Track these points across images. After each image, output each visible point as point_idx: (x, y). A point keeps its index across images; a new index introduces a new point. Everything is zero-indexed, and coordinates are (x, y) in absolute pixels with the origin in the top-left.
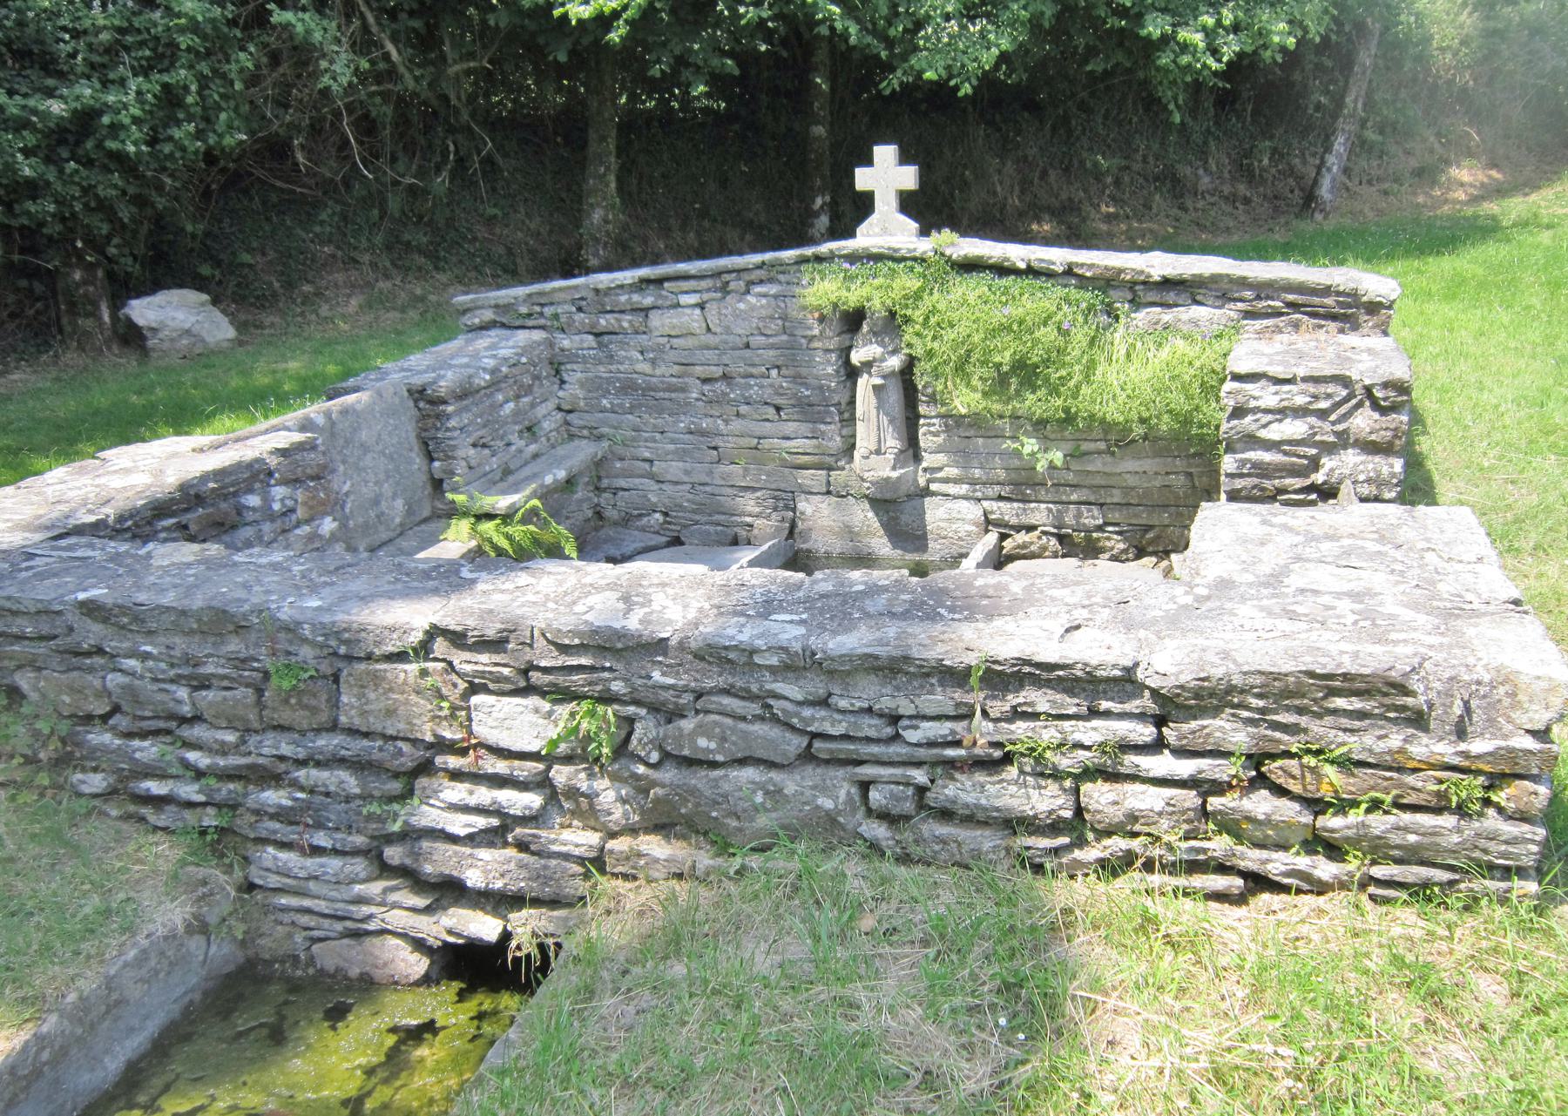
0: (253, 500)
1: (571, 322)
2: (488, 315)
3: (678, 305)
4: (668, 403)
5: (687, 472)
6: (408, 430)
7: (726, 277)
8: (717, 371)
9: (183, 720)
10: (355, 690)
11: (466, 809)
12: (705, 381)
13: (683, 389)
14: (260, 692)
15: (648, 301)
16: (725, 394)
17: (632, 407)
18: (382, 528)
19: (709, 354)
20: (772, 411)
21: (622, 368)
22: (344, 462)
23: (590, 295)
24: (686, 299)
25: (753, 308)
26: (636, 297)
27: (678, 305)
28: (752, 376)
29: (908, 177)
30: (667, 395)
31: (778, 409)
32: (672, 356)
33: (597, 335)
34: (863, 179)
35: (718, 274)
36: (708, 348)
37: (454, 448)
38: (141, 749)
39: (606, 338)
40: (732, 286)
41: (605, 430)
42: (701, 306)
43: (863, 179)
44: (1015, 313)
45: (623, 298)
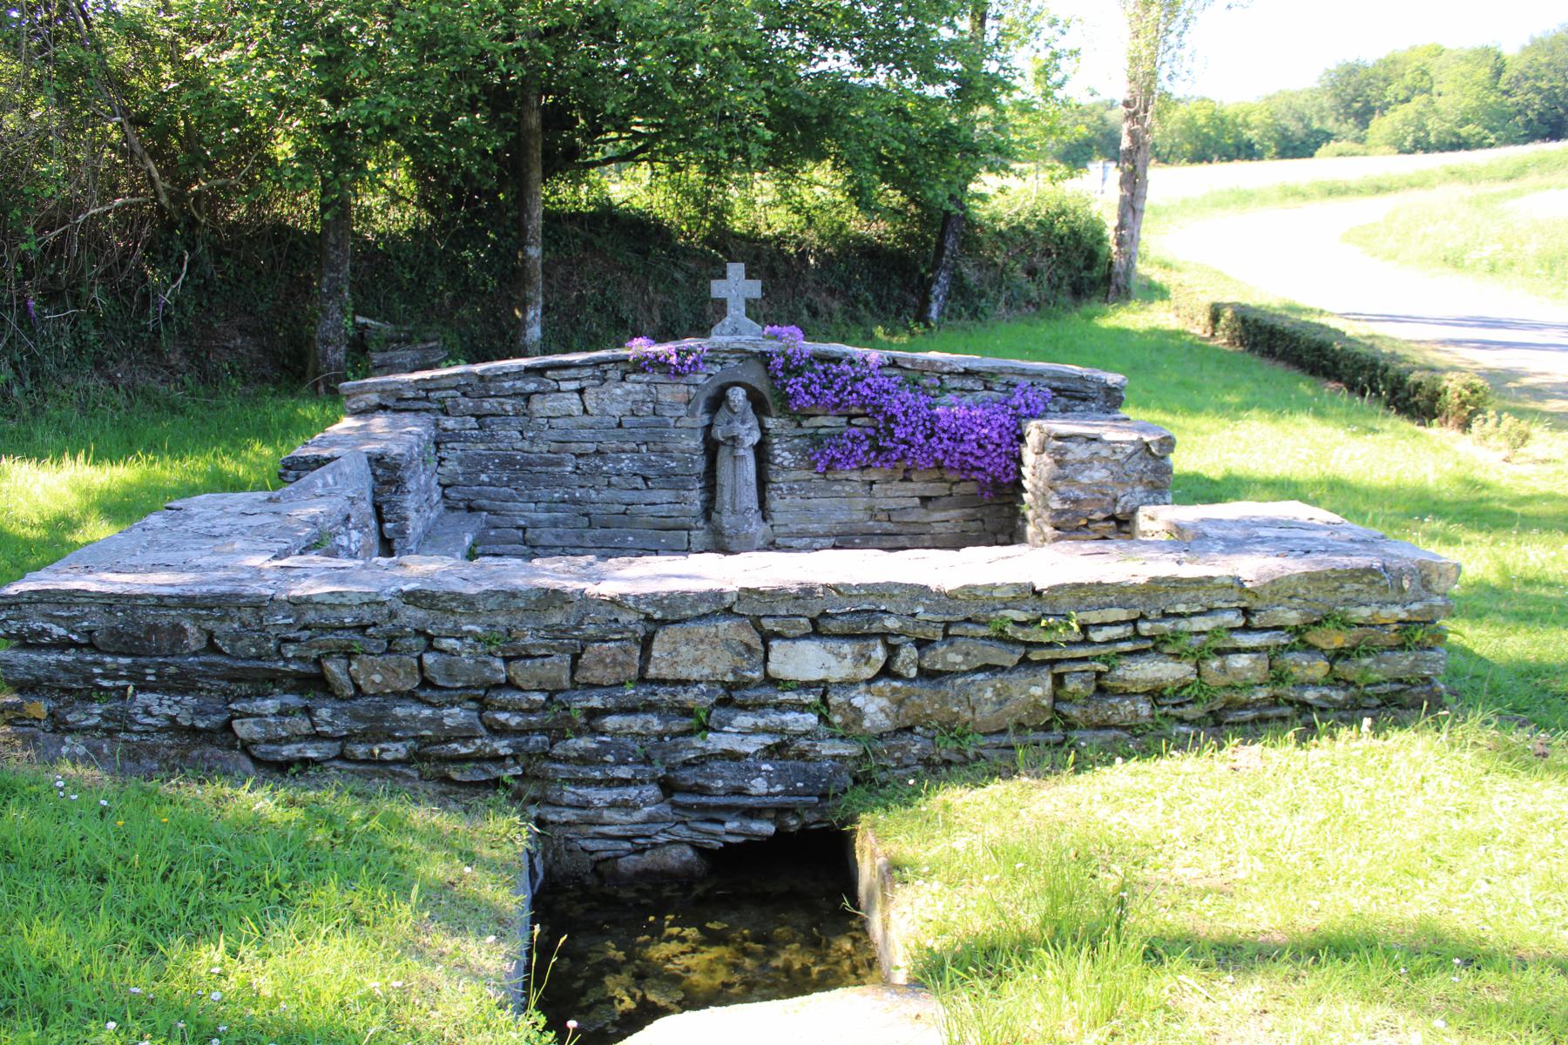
2: (374, 398)
3: (559, 391)
4: (544, 476)
5: (557, 536)
7: (606, 367)
8: (591, 448)
9: (498, 686)
10: (667, 646)
11: (755, 731)
12: (579, 456)
14: (576, 658)
15: (532, 387)
16: (597, 467)
17: (510, 480)
19: (585, 433)
20: (640, 480)
21: (501, 446)
23: (475, 381)
24: (564, 386)
25: (629, 393)
26: (519, 384)
27: (559, 391)
28: (624, 451)
29: (755, 289)
30: (544, 469)
31: (646, 479)
32: (554, 435)
33: (478, 417)
34: (718, 288)
35: (597, 364)
36: (583, 427)
38: (449, 716)
39: (488, 420)
40: (610, 374)
43: (718, 288)
45: (507, 385)
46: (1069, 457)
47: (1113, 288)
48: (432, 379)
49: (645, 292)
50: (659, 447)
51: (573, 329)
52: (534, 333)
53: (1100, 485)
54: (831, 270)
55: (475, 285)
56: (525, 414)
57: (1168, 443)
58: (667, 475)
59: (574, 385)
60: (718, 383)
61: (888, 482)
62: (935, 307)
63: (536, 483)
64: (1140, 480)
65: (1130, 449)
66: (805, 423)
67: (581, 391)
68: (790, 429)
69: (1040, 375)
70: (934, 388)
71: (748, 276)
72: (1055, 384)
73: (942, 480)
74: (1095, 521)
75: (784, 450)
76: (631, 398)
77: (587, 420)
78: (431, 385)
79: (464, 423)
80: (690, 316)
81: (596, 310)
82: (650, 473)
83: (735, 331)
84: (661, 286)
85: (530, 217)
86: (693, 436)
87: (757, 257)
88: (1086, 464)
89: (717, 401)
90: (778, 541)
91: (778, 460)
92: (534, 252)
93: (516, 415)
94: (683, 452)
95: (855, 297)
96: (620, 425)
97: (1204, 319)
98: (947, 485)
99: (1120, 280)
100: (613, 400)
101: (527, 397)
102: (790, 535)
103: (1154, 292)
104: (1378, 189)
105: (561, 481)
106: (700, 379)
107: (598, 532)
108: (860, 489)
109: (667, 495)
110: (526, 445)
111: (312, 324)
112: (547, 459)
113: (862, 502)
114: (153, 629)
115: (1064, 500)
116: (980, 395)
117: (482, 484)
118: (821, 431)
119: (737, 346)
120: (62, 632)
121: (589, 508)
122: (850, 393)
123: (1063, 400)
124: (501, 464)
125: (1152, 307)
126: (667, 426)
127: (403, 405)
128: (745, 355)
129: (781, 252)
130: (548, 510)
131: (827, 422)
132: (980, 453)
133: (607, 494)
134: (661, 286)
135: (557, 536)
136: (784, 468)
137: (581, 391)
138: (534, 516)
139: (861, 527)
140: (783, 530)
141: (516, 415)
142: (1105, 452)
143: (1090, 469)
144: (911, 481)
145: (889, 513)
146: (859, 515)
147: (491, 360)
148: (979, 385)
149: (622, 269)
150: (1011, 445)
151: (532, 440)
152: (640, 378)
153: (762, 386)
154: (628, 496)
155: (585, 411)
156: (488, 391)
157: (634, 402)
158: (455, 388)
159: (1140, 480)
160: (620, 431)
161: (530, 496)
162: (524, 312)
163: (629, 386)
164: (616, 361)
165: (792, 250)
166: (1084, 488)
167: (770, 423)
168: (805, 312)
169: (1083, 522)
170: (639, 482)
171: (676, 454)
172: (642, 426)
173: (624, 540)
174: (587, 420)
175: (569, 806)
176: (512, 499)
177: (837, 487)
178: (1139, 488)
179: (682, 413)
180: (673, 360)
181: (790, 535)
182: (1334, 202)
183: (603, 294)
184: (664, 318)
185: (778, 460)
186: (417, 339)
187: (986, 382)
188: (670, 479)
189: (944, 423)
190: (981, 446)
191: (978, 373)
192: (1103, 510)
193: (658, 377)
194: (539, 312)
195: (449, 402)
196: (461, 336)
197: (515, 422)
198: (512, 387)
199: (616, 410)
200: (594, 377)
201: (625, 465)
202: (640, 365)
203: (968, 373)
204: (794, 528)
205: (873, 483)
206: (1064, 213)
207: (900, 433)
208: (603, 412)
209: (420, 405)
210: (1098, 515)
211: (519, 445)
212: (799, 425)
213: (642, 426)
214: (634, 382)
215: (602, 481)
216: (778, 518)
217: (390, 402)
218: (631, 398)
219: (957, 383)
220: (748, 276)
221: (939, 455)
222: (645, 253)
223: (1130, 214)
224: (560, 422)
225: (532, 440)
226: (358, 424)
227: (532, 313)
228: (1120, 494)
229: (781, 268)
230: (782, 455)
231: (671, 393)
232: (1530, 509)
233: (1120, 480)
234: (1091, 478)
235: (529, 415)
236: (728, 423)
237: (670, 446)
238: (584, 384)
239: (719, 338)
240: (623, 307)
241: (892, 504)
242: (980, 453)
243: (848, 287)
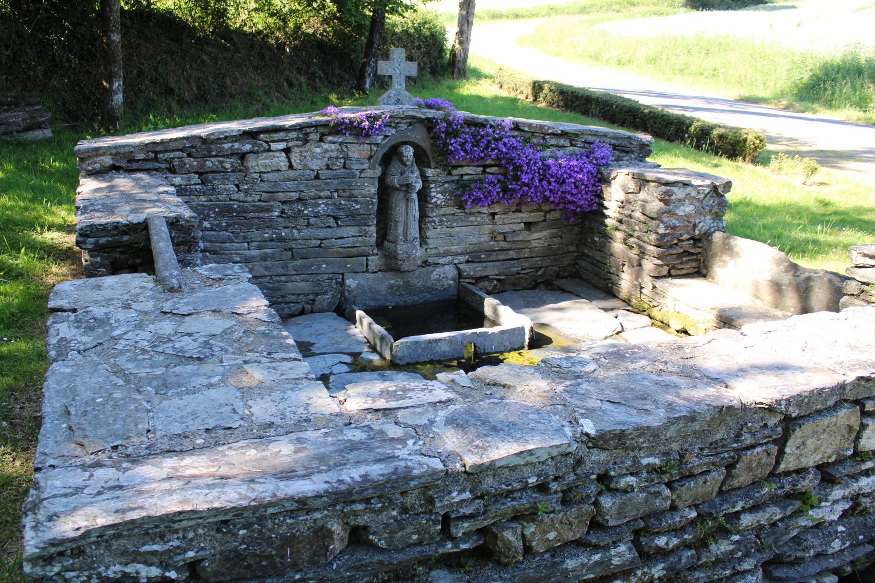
2: (108, 161)
3: (269, 150)
4: (256, 221)
5: (267, 268)
7: (308, 130)
8: (295, 196)
15: (248, 147)
16: (300, 211)
17: (228, 225)
19: (290, 184)
20: (332, 220)
21: (221, 197)
23: (198, 144)
24: (274, 146)
25: (326, 151)
26: (236, 145)
28: (320, 198)
31: (336, 219)
32: (265, 187)
33: (200, 174)
34: (384, 68)
36: (288, 180)
39: (210, 176)
43: (384, 68)
45: (226, 146)
46: (673, 197)
47: (456, 70)
48: (163, 142)
49: (184, 69)
50: (347, 194)
51: (137, 96)
53: (688, 216)
54: (297, 56)
55: (61, 61)
56: (241, 169)
57: (728, 185)
59: (282, 145)
60: (393, 143)
61: (506, 213)
62: (368, 81)
63: (249, 227)
64: (710, 211)
65: (707, 190)
66: (454, 172)
67: (287, 151)
68: (443, 177)
69: (605, 135)
72: (613, 142)
73: (539, 210)
74: (683, 241)
75: (438, 192)
76: (327, 155)
79: (189, 179)
80: (216, 86)
81: (151, 81)
82: (341, 214)
83: (398, 101)
84: (194, 65)
85: (111, 11)
86: (373, 184)
87: (252, 46)
89: (391, 156)
91: (434, 200)
92: (116, 37)
93: (233, 171)
94: (365, 197)
95: (313, 74)
96: (317, 177)
97: (529, 91)
98: (542, 214)
99: (460, 65)
100: (313, 157)
101: (243, 156)
102: (438, 255)
103: (479, 75)
104: (517, 16)
105: (270, 224)
106: (379, 139)
107: (299, 262)
108: (487, 219)
109: (352, 231)
110: (241, 196)
112: (259, 206)
113: (487, 228)
114: (290, 540)
115: (667, 228)
117: (206, 229)
118: (465, 178)
120: (155, 572)
121: (292, 244)
122: (493, 150)
123: (617, 153)
124: (220, 212)
125: (480, 82)
126: (354, 177)
127: (135, 166)
128: (414, 121)
129: (266, 43)
130: (259, 248)
131: (470, 171)
132: (575, 191)
133: (306, 232)
134: (194, 65)
135: (267, 268)
136: (437, 206)
137: (287, 151)
138: (247, 253)
139: (486, 246)
140: (433, 251)
141: (233, 171)
142: (694, 194)
143: (683, 205)
144: (520, 211)
145: (505, 236)
146: (485, 238)
148: (567, 143)
149: (166, 53)
150: (594, 185)
151: (246, 192)
152: (335, 139)
153: (425, 144)
154: (322, 233)
155: (291, 167)
156: (210, 151)
158: (182, 150)
159: (710, 211)
160: (318, 182)
161: (245, 238)
162: (111, 83)
163: (326, 146)
164: (317, 126)
165: (273, 42)
166: (679, 218)
167: (430, 172)
168: (285, 84)
169: (675, 242)
171: (360, 199)
172: (335, 177)
173: (319, 267)
174: (292, 174)
177: (472, 219)
179: (366, 166)
180: (366, 124)
181: (438, 255)
182: (495, 22)
183: (156, 70)
184: (199, 88)
185: (434, 200)
186: (23, 104)
187: (571, 140)
188: (355, 218)
189: (554, 170)
190: (576, 187)
192: (688, 233)
193: (349, 138)
194: (121, 83)
195: (176, 162)
196: (55, 101)
197: (233, 177)
198: (230, 148)
199: (316, 164)
200: (298, 139)
201: (322, 209)
202: (338, 128)
203: (564, 134)
204: (441, 250)
205: (496, 214)
206: (425, 23)
207: (525, 179)
208: (306, 167)
209: (150, 165)
210: (686, 236)
211: (236, 196)
212: (450, 173)
213: (335, 177)
215: (302, 222)
216: (432, 243)
217: (123, 164)
218: (327, 155)
219: (554, 141)
221: (547, 193)
222: (179, 41)
223: (466, 25)
224: (270, 176)
225: (246, 192)
226: (104, 185)
227: (117, 84)
228: (697, 221)
229: (267, 54)
230: (437, 197)
231: (358, 151)
232: (866, 217)
233: (699, 212)
234: (684, 211)
235: (245, 171)
236: (402, 174)
237: (356, 192)
238: (290, 144)
240: (171, 80)
241: (507, 228)
242: (575, 191)
243: (309, 67)
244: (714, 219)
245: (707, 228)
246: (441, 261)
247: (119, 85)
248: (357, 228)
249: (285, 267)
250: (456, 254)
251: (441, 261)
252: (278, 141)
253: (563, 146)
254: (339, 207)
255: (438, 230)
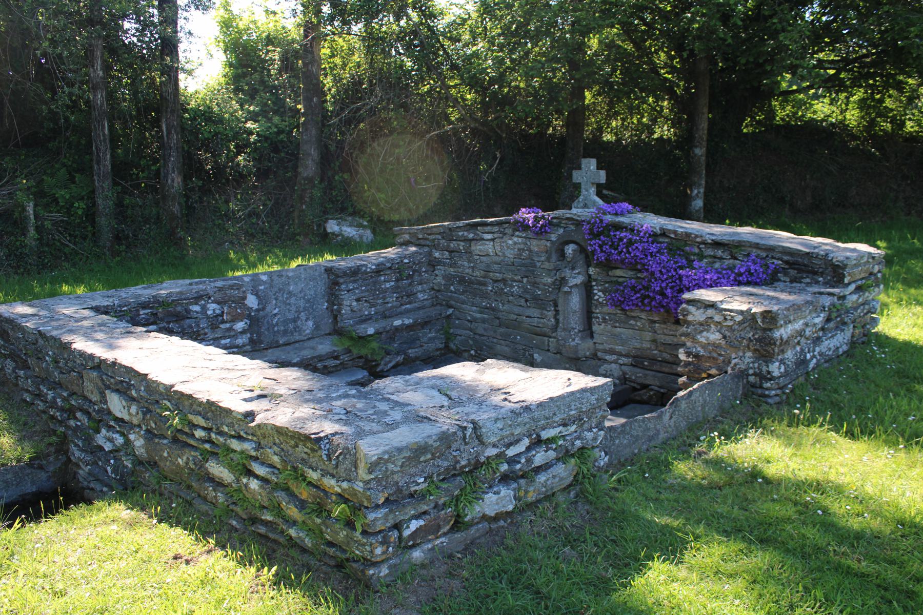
0: (196, 308)
1: (439, 244)
5: (485, 330)
6: (321, 287)
12: (496, 281)
13: (484, 284)
15: (471, 236)
18: (296, 334)
20: (523, 300)
22: (276, 299)
23: (447, 231)
25: (515, 243)
28: (515, 281)
31: (526, 301)
37: (343, 299)
41: (453, 303)
42: (493, 240)
43: (577, 176)
44: (903, 246)
45: (460, 234)
52: (699, 203)
53: (716, 346)
58: (536, 299)
61: (665, 323)
65: (739, 318)
70: (695, 254)
71: (580, 168)
72: (785, 258)
75: (599, 291)
77: (497, 259)
78: (429, 232)
79: (443, 255)
88: (705, 325)
90: (599, 354)
91: (596, 297)
94: (545, 285)
105: (485, 296)
111: (558, 194)
113: (648, 336)
116: (727, 262)
119: (568, 216)
123: (793, 272)
135: (485, 330)
136: (600, 303)
141: (466, 252)
142: (718, 318)
143: (708, 331)
147: (721, 221)
148: (726, 255)
154: (516, 310)
157: (519, 250)
158: (439, 234)
163: (515, 239)
170: (522, 302)
171: (541, 286)
175: (257, 477)
176: (463, 303)
177: (632, 322)
178: (749, 354)
185: (596, 297)
191: (727, 245)
204: (607, 347)
214: (518, 236)
216: (597, 338)
219: (710, 252)
220: (580, 168)
234: (707, 339)
239: (576, 211)
244: (757, 359)
245: (743, 367)
246: (608, 357)
247: (699, 192)
248: (539, 311)
249: (495, 332)
250: (620, 354)
251: (608, 357)
252: (488, 233)
253: (721, 258)
254: (526, 291)
255: (602, 327)
